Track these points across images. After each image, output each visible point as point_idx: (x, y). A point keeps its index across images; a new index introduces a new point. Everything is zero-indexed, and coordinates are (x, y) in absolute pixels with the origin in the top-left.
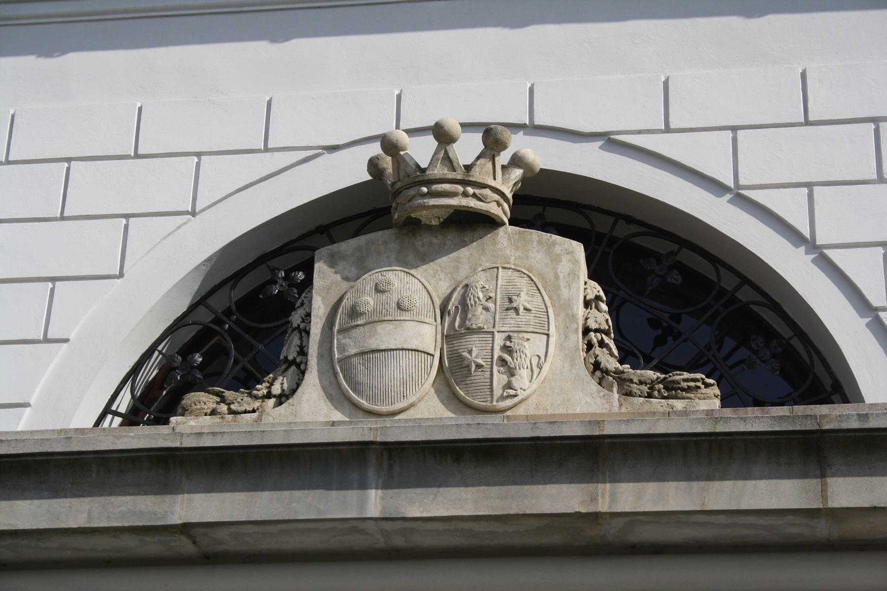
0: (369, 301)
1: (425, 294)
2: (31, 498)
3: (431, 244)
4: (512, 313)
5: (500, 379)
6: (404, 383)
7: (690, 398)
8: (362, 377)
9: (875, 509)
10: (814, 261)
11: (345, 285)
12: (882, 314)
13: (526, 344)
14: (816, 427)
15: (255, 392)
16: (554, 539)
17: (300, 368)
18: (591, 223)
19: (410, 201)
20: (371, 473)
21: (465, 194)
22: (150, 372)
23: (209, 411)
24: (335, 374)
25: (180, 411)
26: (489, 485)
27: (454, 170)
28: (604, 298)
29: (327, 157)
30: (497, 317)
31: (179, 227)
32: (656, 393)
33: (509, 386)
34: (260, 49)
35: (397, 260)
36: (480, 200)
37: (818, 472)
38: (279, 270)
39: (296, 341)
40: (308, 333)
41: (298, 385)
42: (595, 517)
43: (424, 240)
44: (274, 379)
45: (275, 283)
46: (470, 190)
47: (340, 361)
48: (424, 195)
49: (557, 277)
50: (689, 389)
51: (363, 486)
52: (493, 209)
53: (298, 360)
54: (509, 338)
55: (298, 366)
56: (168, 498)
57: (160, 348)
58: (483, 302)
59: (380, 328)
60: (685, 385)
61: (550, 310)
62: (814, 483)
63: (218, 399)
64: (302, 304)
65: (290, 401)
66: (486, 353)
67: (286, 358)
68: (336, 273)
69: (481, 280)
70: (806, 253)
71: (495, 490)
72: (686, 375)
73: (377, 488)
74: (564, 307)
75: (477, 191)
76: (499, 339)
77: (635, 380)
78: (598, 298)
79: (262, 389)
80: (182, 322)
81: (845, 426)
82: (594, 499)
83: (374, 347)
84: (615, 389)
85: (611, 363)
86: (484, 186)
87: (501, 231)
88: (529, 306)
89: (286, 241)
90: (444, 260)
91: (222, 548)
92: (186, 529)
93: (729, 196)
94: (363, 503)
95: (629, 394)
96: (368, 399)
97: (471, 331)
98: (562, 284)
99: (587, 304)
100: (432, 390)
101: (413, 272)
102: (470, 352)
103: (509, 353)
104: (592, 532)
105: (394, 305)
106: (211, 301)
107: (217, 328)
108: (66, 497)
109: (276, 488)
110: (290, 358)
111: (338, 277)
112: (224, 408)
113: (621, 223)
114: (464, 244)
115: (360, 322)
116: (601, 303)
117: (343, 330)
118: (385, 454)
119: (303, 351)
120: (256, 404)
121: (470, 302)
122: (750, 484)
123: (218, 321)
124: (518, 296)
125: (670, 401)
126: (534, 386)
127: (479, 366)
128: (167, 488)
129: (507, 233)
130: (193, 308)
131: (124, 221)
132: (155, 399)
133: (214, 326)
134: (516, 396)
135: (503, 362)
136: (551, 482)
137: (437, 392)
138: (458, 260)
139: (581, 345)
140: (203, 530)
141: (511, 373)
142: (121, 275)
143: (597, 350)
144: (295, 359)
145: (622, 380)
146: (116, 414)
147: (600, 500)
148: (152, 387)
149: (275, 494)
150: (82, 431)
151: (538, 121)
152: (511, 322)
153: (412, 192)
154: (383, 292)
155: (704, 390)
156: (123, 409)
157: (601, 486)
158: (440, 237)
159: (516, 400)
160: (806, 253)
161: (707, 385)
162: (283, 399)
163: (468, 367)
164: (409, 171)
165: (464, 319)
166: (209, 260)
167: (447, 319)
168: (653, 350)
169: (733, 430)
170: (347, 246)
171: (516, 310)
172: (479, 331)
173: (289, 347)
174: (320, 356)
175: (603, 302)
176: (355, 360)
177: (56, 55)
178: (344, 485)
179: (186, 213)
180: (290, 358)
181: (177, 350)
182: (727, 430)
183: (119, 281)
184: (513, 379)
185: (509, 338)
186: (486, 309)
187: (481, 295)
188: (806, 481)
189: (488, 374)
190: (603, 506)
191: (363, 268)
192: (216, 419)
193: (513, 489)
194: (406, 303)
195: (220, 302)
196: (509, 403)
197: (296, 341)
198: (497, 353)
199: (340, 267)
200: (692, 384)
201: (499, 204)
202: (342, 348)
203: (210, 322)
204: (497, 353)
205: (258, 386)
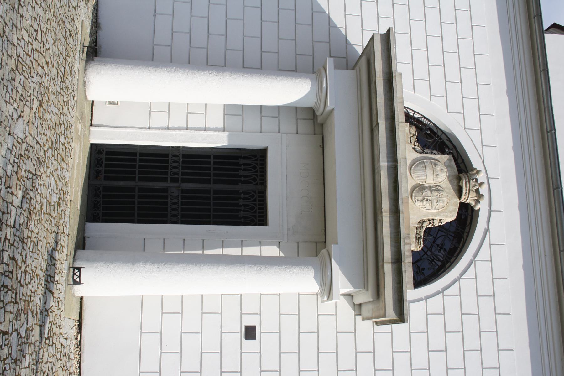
0: (438, 168)
1: (441, 181)
2: (383, 90)
3: (454, 183)
4: (436, 201)
5: (420, 198)
6: (418, 176)
7: (416, 243)
8: (419, 166)
9: (384, 274)
10: (456, 278)
11: (443, 163)
12: (442, 293)
13: (428, 204)
14: (402, 261)
15: (416, 142)
16: (378, 206)
17: (423, 152)
18: (468, 226)
19: (464, 177)
20: (391, 163)
21: (466, 190)
22: (426, 122)
23: (411, 132)
24: (420, 160)
25: (411, 125)
26: (388, 189)
27: (473, 187)
28: (442, 224)
29: (481, 161)
30: (435, 198)
31: (461, 125)
32: (417, 235)
33: (418, 200)
35: (450, 175)
36: (465, 194)
37: (392, 262)
38: (452, 151)
39: (429, 152)
40: (431, 154)
41: (418, 152)
42: (382, 213)
43: (455, 181)
44: (419, 147)
45: (448, 150)
46: (468, 191)
47: (423, 161)
48: (466, 180)
49: (446, 212)
50: (418, 243)
51: (388, 162)
53: (424, 152)
54: (430, 200)
55: (423, 152)
56: (384, 119)
57: (431, 123)
58: (439, 195)
59: (432, 170)
60: (420, 242)
61: (438, 211)
62: (390, 261)
63: (414, 134)
64: (438, 153)
65: (413, 150)
66: (426, 195)
67: (425, 149)
68: (446, 160)
69: (445, 194)
70: (458, 277)
71: (387, 191)
72: (422, 243)
73: (387, 165)
74: (438, 214)
75: (467, 193)
76: (429, 198)
78: (442, 223)
79: (417, 144)
80: (438, 129)
81: (403, 267)
82: (385, 212)
83: (427, 169)
84: (418, 226)
85: (425, 225)
86: (469, 195)
87: (458, 199)
88: (438, 205)
89: (460, 152)
90: (450, 186)
91: (374, 133)
92: (377, 124)
93: (473, 259)
94: (384, 161)
95: (417, 229)
96: (414, 168)
97: (431, 191)
98: (444, 214)
99: (440, 220)
100: (416, 183)
101: (447, 178)
102: (426, 191)
104: (379, 213)
105: (438, 174)
106: (443, 135)
107: (436, 136)
108: (384, 97)
109: (387, 143)
110: (425, 150)
111: (445, 161)
112: (412, 135)
113: (467, 234)
114: (454, 191)
115: (433, 166)
116: (440, 223)
117: (431, 162)
118: (395, 166)
119: (426, 153)
120: (413, 143)
121: (439, 192)
122: (390, 247)
123: (438, 136)
124: (441, 203)
125: (415, 238)
126: (418, 206)
127: (423, 193)
128: (386, 119)
129: (457, 201)
130: (442, 131)
131: (462, 112)
132: (419, 124)
133: (437, 135)
134: (416, 202)
135: (424, 199)
136: (389, 203)
137: (416, 184)
138: (450, 189)
139: (430, 218)
140: (377, 128)
141: (421, 201)
142: (448, 113)
143: (429, 222)
144: (424, 151)
145: (421, 227)
146: (414, 114)
147: (385, 213)
148: (422, 122)
149: (386, 142)
150: (403, 102)
151: (492, 212)
152: (434, 200)
153: (467, 177)
154: (441, 171)
155: (418, 246)
156: (415, 116)
157: (389, 214)
158: (456, 185)
159: (415, 202)
160: (458, 277)
161: (420, 247)
162: (414, 149)
163: (422, 191)
164: (472, 177)
165: (434, 190)
166: (453, 133)
167: (435, 186)
168: (436, 244)
169: (402, 243)
170: (453, 163)
171: (437, 202)
172: (431, 193)
173: (427, 150)
174: (425, 157)
175: (441, 224)
176: (424, 165)
179: (465, 127)
180: (425, 150)
181: (431, 127)
182: (401, 241)
183: (447, 112)
184: (420, 201)
185: (430, 200)
186: (437, 195)
187: (441, 194)
188: (390, 259)
189: (421, 195)
190: (384, 214)
192: (409, 134)
193: (387, 194)
194: (438, 176)
195: (443, 137)
196: (414, 201)
197: (429, 152)
198: (426, 198)
199: (447, 161)
200: (420, 243)
201: (465, 199)
202: (426, 162)
203: (438, 135)
204: (426, 198)
205: (417, 143)
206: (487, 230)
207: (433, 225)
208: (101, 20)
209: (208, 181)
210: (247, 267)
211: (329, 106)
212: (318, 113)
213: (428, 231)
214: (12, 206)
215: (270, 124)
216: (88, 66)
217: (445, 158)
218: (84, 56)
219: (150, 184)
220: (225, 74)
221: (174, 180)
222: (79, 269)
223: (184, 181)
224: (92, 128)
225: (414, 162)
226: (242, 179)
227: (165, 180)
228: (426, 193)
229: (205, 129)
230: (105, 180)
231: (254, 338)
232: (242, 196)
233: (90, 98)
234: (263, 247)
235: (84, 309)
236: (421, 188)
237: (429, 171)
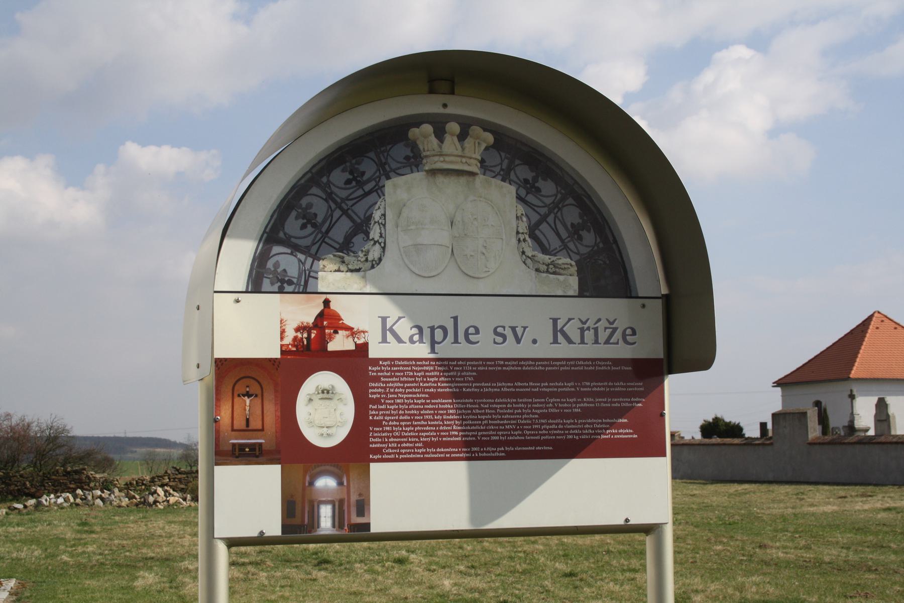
19: (435, 163)
36: (469, 165)
46: (464, 160)
60: (563, 266)
77: (541, 262)
86: (471, 158)
103: (675, 539)
159: (490, 273)
168: (526, 196)
200: (566, 266)
207: (526, 233)
230: (197, 501)
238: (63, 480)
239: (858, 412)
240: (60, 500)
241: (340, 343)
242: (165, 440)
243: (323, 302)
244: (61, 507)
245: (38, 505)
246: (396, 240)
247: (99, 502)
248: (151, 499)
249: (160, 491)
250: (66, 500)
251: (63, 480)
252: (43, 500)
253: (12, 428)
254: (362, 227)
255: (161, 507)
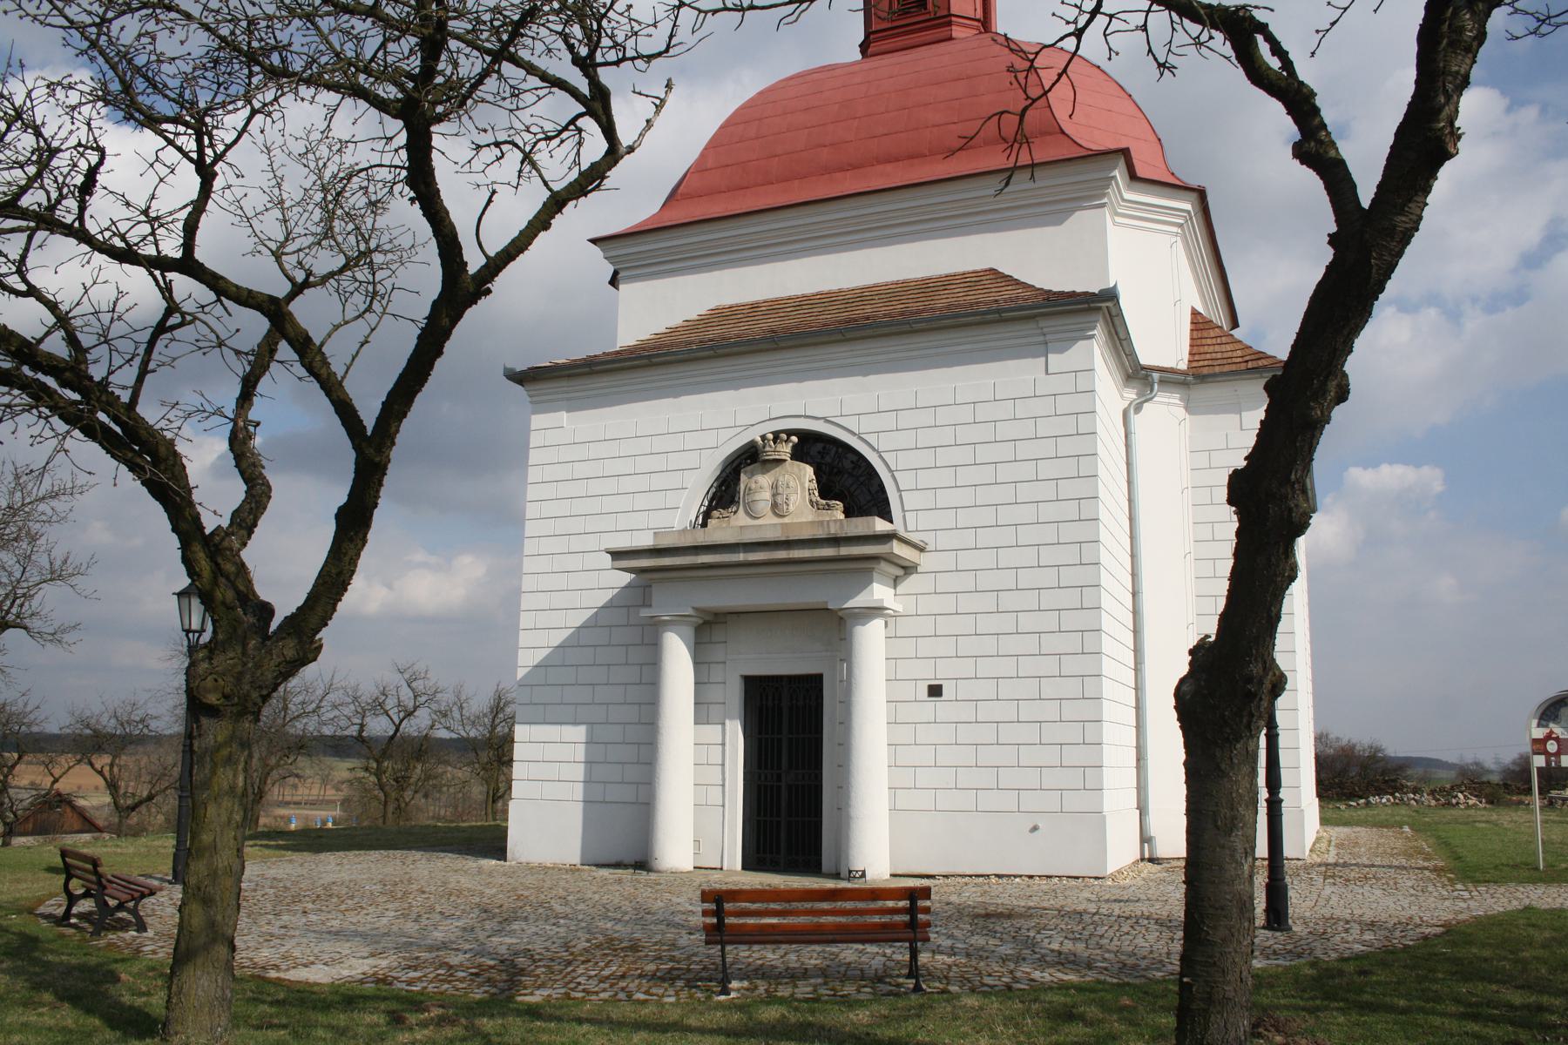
0: (753, 486)
22: (713, 490)
34: (732, 393)
43: (768, 465)
52: (783, 457)
62: (836, 549)
69: (781, 479)
128: (697, 554)
148: (714, 494)
177: (393, 429)
178: (735, 553)
191: (753, 475)
206: (826, 420)
208: (613, 861)
209: (780, 740)
210: (853, 699)
211: (690, 612)
212: (701, 621)
213: (822, 496)
214: (85, 344)
215: (717, 673)
216: (655, 868)
217: (743, 477)
218: (645, 873)
219: (784, 804)
220: (660, 725)
221: (779, 778)
222: (850, 872)
223: (779, 768)
224: (725, 868)
225: (747, 513)
226: (776, 702)
227: (779, 788)
228: (779, 499)
229: (723, 744)
231: (940, 687)
232: (794, 702)
233: (692, 869)
234: (582, 765)
235: (910, 873)
236: (775, 506)
237: (757, 497)
238: (1383, 786)
239: (479, 703)
240: (1384, 800)
241: (1554, 736)
242: (1437, 760)
243: (1191, 652)
244: (1384, 805)
245: (1368, 804)
246: (1563, 718)
247: (1413, 802)
248: (1454, 801)
249: (1460, 795)
250: (1388, 800)
251: (1383, 786)
252: (1371, 799)
253: (1343, 749)
254: (1557, 717)
255: (1462, 807)
